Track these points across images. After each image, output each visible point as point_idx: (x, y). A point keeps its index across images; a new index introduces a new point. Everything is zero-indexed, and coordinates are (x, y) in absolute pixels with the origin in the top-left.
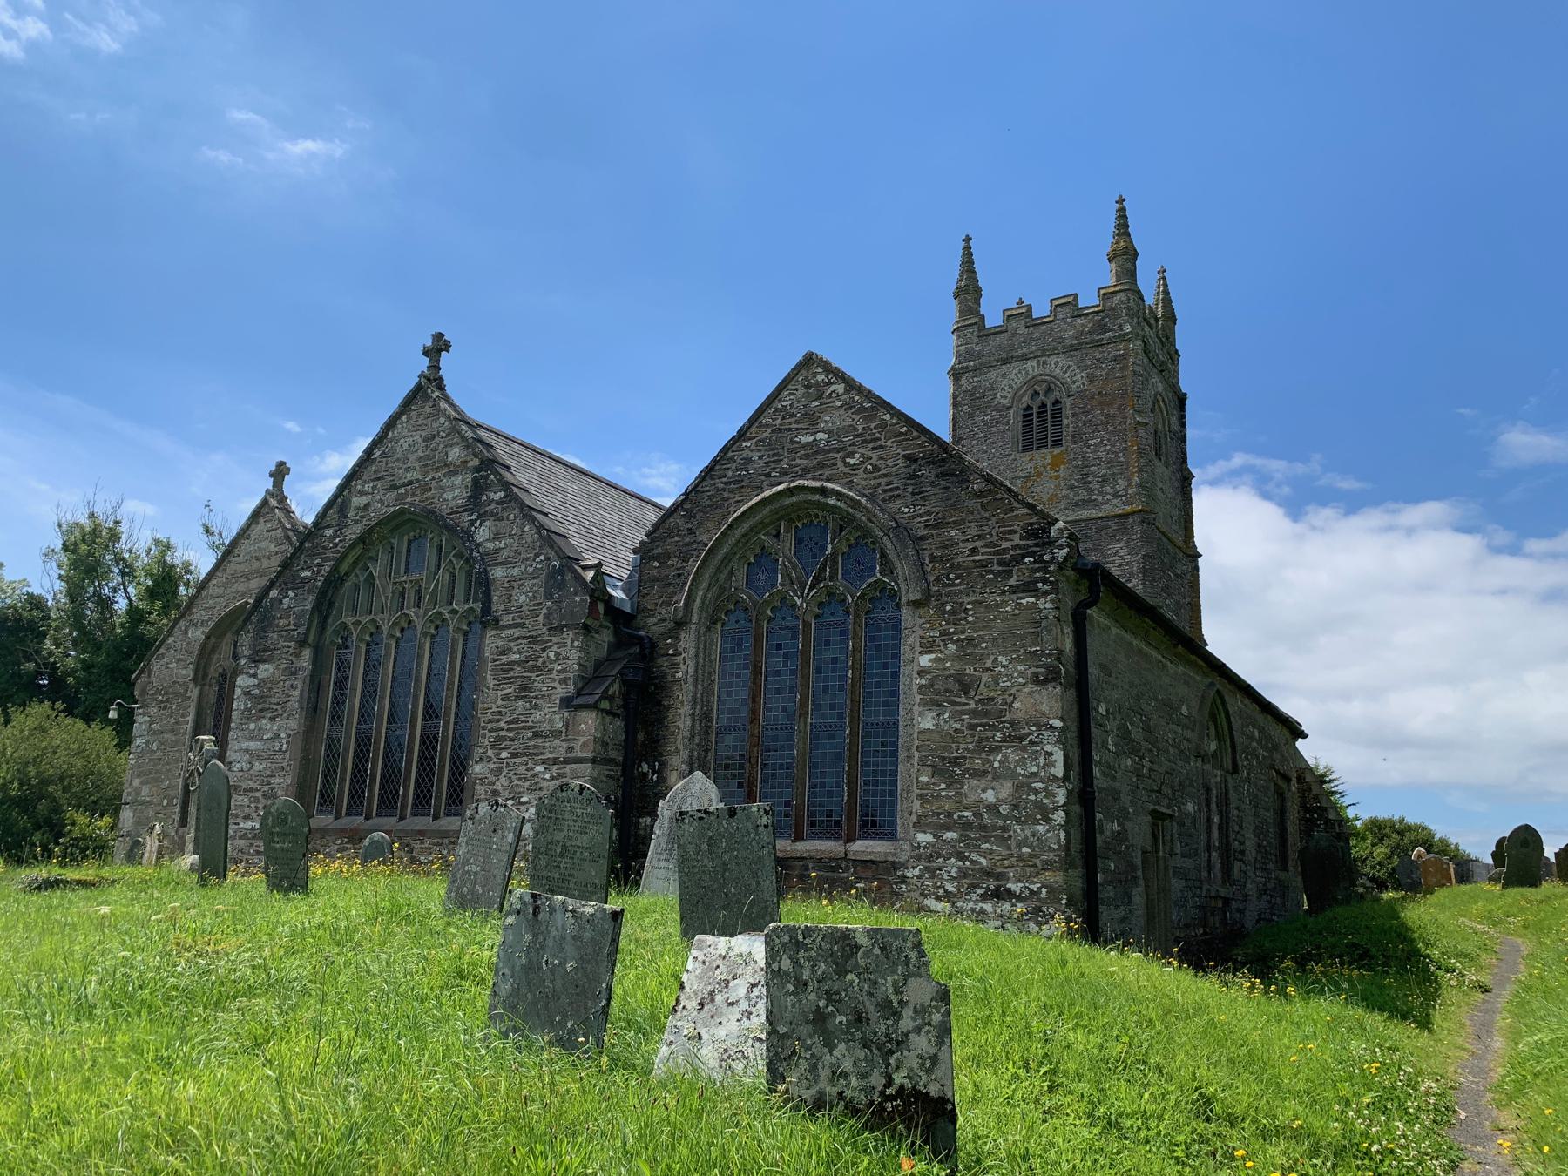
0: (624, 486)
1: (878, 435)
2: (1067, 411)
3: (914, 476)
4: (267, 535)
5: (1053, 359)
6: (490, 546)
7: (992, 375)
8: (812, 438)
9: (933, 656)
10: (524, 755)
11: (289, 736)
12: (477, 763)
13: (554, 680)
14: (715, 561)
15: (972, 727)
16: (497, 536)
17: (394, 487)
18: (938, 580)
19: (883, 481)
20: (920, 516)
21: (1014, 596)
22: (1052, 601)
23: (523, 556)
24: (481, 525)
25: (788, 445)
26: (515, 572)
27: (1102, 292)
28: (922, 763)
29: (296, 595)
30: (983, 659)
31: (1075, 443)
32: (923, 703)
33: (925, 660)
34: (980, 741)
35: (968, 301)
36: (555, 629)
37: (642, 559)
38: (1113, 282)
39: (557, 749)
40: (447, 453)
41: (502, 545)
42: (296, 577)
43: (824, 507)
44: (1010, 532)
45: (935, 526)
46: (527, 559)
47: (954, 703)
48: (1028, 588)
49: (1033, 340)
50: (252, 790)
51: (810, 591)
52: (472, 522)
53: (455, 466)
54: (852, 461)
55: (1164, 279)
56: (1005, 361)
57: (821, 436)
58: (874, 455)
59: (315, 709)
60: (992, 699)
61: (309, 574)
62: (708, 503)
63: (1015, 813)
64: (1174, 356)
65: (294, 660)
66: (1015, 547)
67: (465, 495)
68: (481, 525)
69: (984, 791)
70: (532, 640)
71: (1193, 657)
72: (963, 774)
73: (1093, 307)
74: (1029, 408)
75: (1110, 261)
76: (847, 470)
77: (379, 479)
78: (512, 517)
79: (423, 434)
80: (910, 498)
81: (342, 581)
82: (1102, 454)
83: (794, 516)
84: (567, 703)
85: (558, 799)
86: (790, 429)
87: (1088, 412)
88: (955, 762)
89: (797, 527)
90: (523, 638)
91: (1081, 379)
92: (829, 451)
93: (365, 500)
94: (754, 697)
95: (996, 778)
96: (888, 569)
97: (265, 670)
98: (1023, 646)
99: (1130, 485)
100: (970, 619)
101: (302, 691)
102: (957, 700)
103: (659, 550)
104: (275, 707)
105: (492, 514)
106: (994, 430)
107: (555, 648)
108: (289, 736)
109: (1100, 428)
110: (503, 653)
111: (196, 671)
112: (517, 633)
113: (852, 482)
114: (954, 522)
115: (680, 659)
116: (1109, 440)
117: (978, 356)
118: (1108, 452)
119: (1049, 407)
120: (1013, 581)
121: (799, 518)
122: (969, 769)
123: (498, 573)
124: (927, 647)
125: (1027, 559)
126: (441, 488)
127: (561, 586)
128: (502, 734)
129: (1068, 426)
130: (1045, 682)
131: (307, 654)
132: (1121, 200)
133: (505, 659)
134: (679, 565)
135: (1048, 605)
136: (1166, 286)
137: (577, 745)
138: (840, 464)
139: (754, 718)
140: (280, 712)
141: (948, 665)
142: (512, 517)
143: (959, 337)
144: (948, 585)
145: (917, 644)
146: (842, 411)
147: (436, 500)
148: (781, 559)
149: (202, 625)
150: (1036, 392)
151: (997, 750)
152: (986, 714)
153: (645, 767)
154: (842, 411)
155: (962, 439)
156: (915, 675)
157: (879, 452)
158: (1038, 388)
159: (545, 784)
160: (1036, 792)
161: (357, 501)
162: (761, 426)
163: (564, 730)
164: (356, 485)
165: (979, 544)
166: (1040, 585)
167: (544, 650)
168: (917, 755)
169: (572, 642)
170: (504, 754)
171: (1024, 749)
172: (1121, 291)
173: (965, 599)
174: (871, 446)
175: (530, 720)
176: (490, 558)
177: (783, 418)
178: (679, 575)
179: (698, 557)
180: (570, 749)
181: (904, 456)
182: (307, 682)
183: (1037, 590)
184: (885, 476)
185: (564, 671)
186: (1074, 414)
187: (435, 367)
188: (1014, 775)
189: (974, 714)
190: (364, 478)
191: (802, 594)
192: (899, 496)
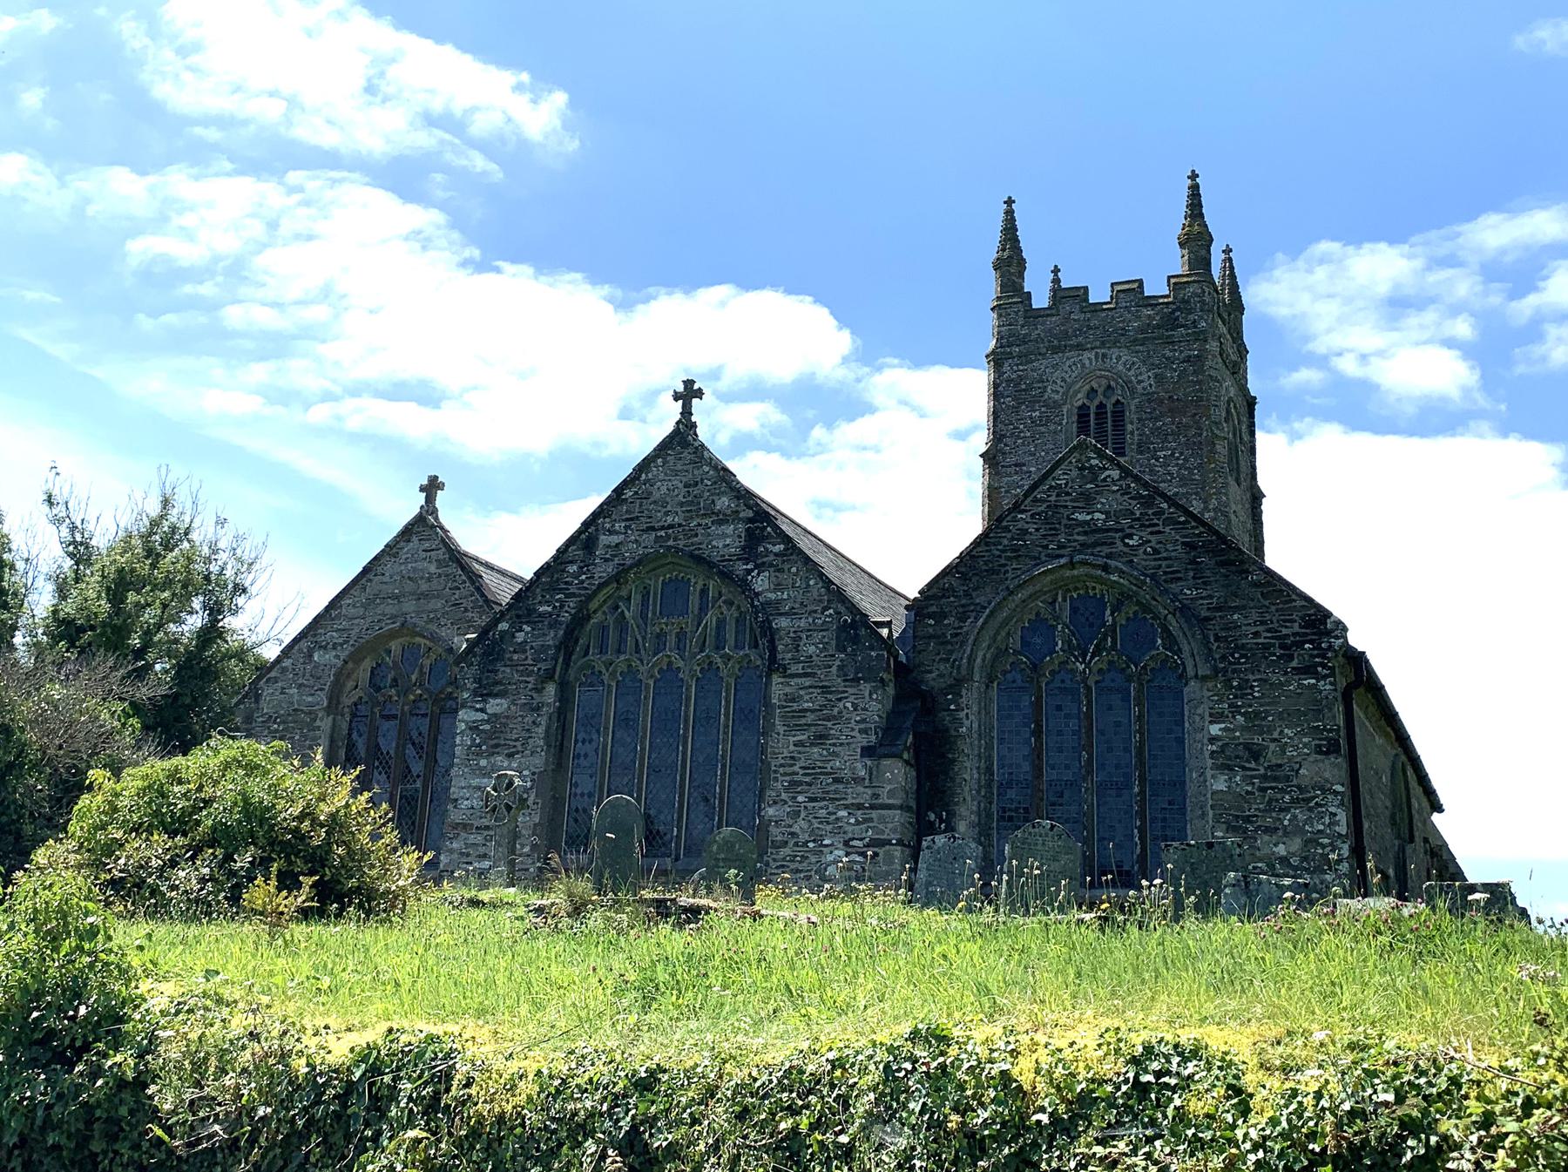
0: (809, 528)
1: (1156, 521)
2: (1131, 415)
3: (1193, 562)
4: (424, 555)
5: (1115, 352)
6: (772, 596)
7: (1041, 364)
8: (1089, 517)
9: (1223, 726)
10: (824, 799)
11: (534, 774)
12: (770, 806)
13: (853, 730)
14: (995, 623)
15: (1263, 790)
16: (778, 587)
17: (653, 529)
18: (1223, 658)
19: (1164, 563)
20: (1202, 598)
21: (1296, 677)
22: (1331, 683)
23: (809, 608)
24: (758, 574)
25: (1064, 521)
26: (803, 623)
27: (1173, 281)
28: (1217, 819)
29: (533, 629)
30: (1270, 732)
31: (1141, 453)
32: (1216, 767)
33: (1215, 729)
34: (1270, 801)
35: (1013, 274)
36: (852, 680)
37: (916, 615)
38: (1185, 270)
39: (864, 794)
40: (713, 501)
41: (785, 596)
42: (531, 611)
43: (1101, 581)
44: (1289, 621)
45: (1219, 609)
46: (815, 612)
47: (1244, 768)
48: (1308, 670)
49: (1089, 328)
50: (487, 828)
51: (1092, 658)
52: (749, 572)
53: (725, 515)
54: (1131, 543)
55: (1230, 260)
56: (1056, 350)
57: (1097, 515)
58: (1153, 538)
59: (561, 750)
60: (1280, 766)
61: (549, 609)
62: (984, 568)
63: (1305, 864)
64: (1242, 351)
65: (535, 695)
66: (1294, 634)
67: (737, 544)
68: (758, 574)
69: (1276, 845)
70: (825, 690)
71: (1389, 729)
72: (1256, 831)
73: (1162, 297)
74: (1083, 407)
75: (1182, 245)
76: (1126, 550)
77: (632, 519)
78: (794, 570)
79: (684, 479)
80: (1191, 582)
81: (589, 617)
82: (1174, 470)
83: (1071, 586)
84: (868, 752)
85: (1030, 834)
86: (1066, 507)
87: (1157, 419)
88: (1248, 819)
89: (1072, 597)
90: (816, 687)
91: (1147, 379)
92: (1108, 530)
93: (615, 539)
94: (1037, 753)
95: (1286, 834)
96: (1171, 642)
97: (496, 705)
98: (1306, 721)
99: (1206, 509)
100: (1256, 694)
101: (548, 728)
102: (1247, 765)
103: (934, 609)
104: (512, 743)
105: (771, 565)
106: (1043, 429)
107: (852, 699)
108: (534, 774)
109: (1170, 438)
110: (793, 700)
111: (330, 700)
112: (807, 682)
113: (1132, 561)
114: (1236, 607)
115: (962, 714)
116: (1181, 454)
117: (1024, 341)
118: (1180, 467)
119: (1109, 408)
120: (1294, 664)
121: (1076, 589)
122: (1260, 826)
123: (782, 623)
124: (1217, 718)
125: (1307, 646)
126: (709, 535)
127: (855, 640)
128: (796, 778)
129: (1132, 433)
130: (1327, 753)
131: (551, 689)
132: (1194, 176)
133: (795, 706)
134: (956, 625)
135: (1328, 687)
136: (1232, 268)
137: (884, 792)
138: (1119, 543)
139: (1038, 771)
140: (520, 749)
141: (1237, 734)
142: (794, 570)
143: (1000, 316)
144: (1234, 664)
145: (1207, 714)
146: (1118, 495)
147: (704, 546)
148: (1060, 627)
149: (334, 648)
150: (1092, 388)
151: (1286, 810)
152: (1276, 779)
153: (932, 817)
154: (1118, 495)
155: (1004, 436)
156: (1205, 741)
157: (1159, 537)
158: (1095, 386)
159: (850, 829)
160: (1323, 846)
161: (604, 539)
162: (1036, 500)
163: (867, 777)
164: (603, 523)
165: (1260, 628)
166: (1320, 669)
167: (840, 700)
168: (1211, 813)
169: (870, 694)
170: (800, 799)
171: (1310, 809)
172: (1194, 282)
173: (1251, 677)
174: (1149, 530)
175: (829, 766)
176: (772, 608)
177: (1058, 495)
178: (957, 635)
179: (976, 619)
180: (876, 796)
181: (1183, 543)
182: (555, 718)
183: (1317, 673)
184: (1166, 559)
185: (863, 721)
186: (1140, 420)
187: (687, 412)
188: (1303, 832)
189: (1264, 778)
190: (614, 517)
191: (1084, 659)
192: (1180, 579)
